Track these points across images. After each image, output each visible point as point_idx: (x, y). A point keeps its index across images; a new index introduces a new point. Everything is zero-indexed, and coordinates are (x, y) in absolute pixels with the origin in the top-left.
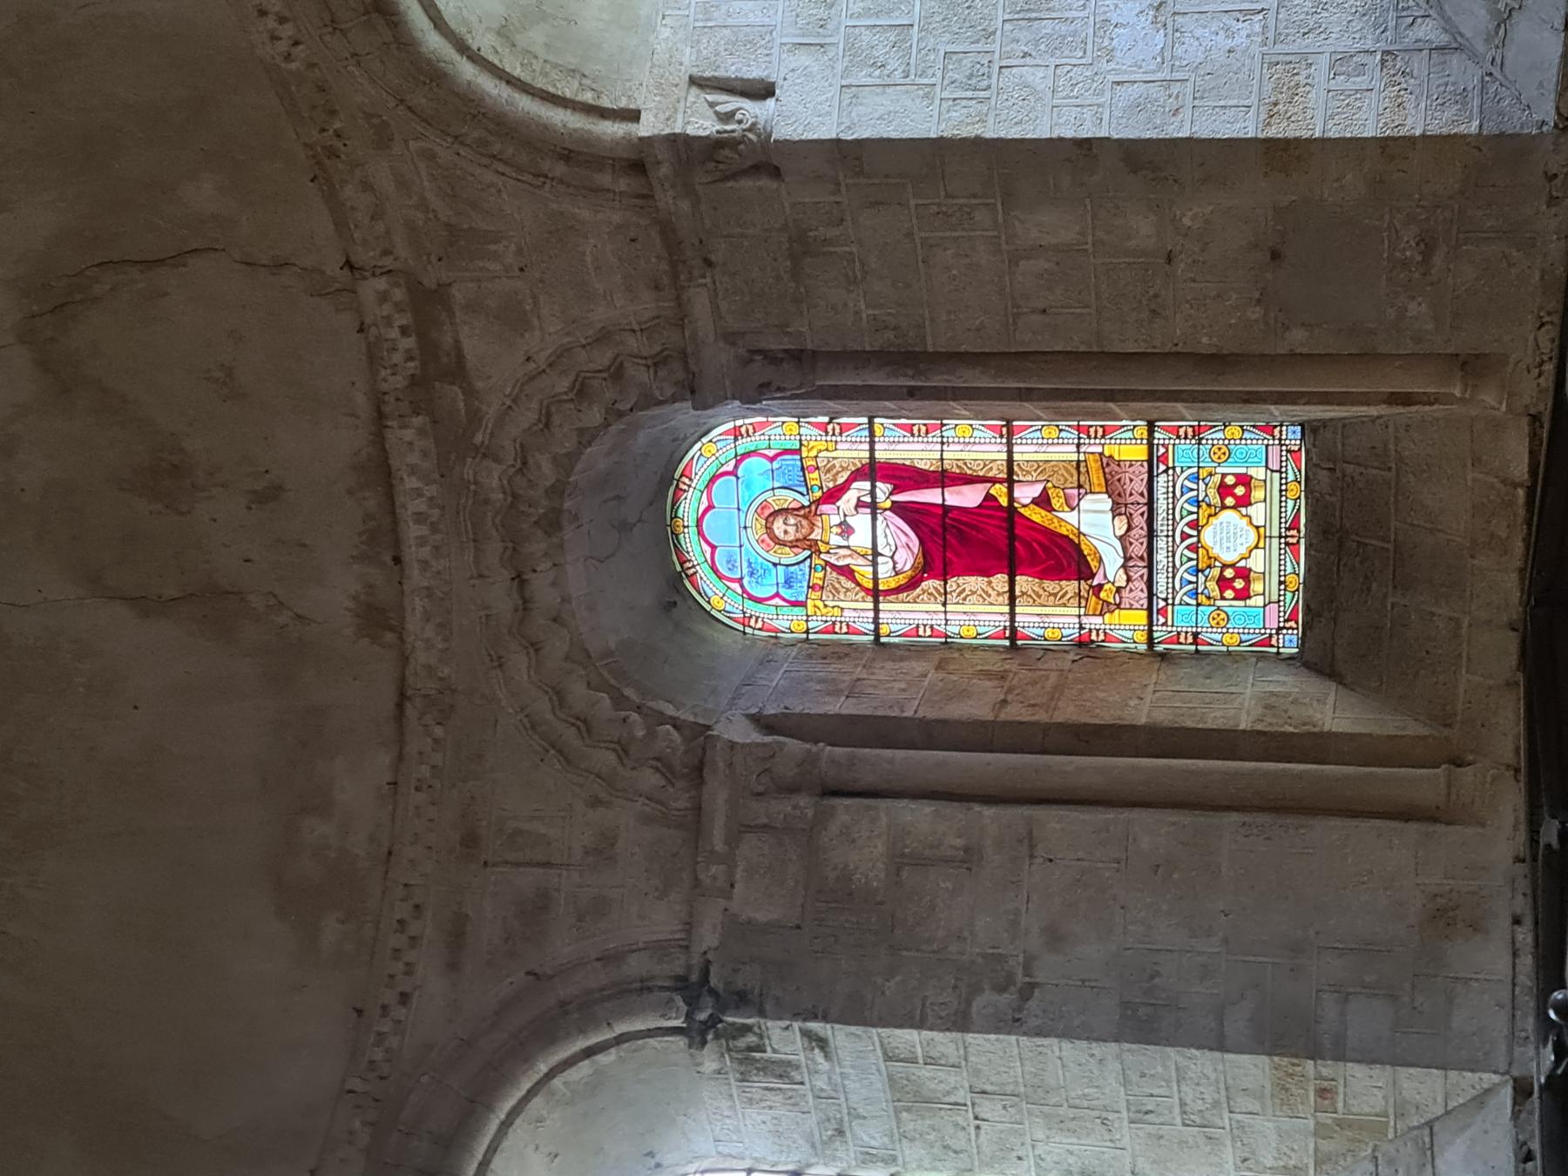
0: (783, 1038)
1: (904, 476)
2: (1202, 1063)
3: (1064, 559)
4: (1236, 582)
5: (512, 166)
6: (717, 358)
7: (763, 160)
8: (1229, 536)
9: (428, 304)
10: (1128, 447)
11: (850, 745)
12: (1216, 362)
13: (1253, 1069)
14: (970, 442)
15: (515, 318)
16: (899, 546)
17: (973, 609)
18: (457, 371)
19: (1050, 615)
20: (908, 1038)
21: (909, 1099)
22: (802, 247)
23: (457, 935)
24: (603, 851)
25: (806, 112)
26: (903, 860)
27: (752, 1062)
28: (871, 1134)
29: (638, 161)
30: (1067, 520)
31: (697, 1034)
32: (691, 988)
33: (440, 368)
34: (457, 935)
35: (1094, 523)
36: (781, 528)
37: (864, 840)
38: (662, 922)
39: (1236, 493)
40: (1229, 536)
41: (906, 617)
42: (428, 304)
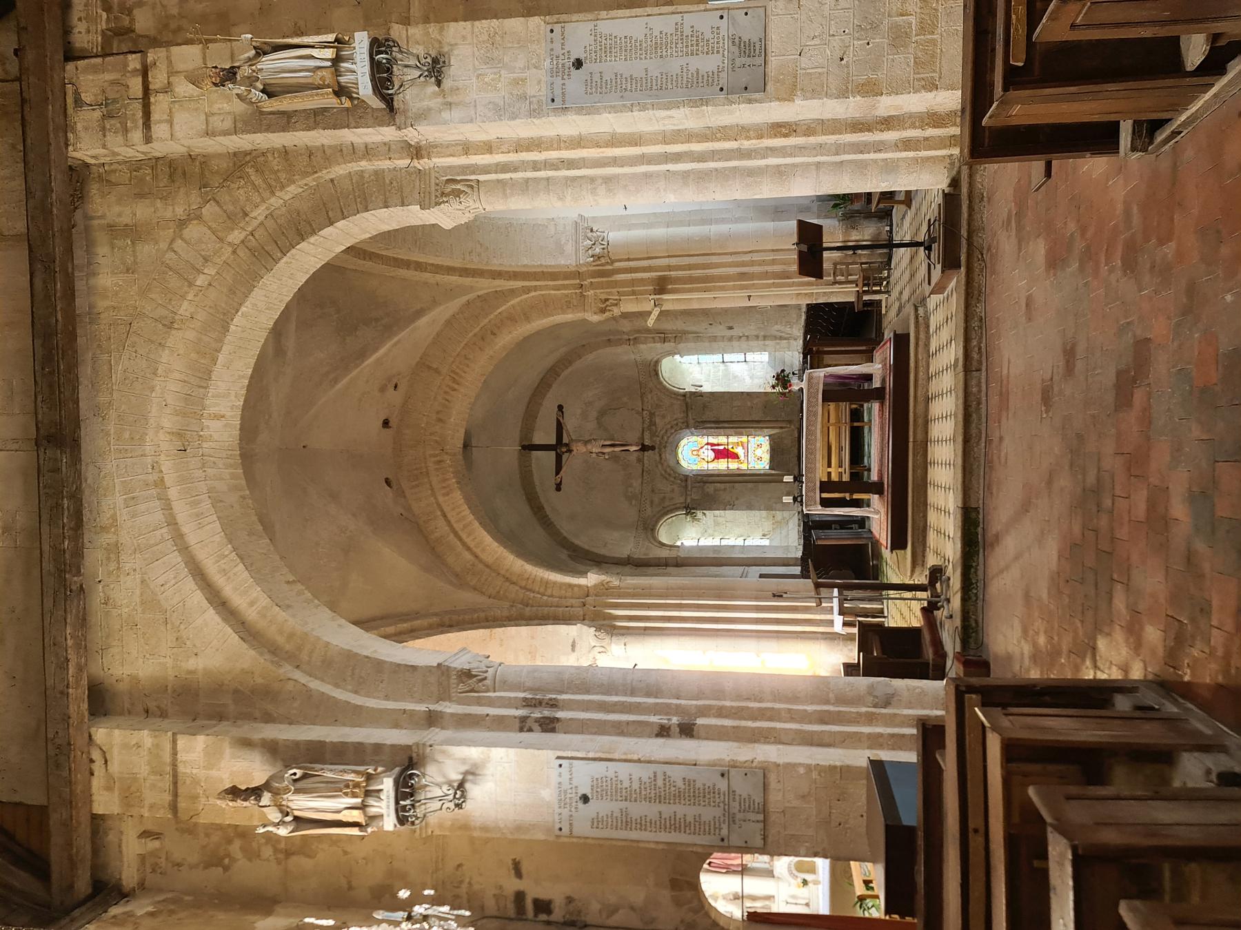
0: (699, 514)
1: (713, 445)
2: (757, 513)
3: (735, 456)
4: (760, 459)
5: (970, 201)
6: (691, 422)
7: (701, 395)
8: (759, 452)
9: (652, 415)
10: (744, 439)
11: (704, 480)
12: (758, 422)
13: (764, 513)
14: (722, 439)
15: (664, 417)
16: (712, 455)
17: (722, 465)
18: (655, 424)
19: (733, 465)
20: (717, 512)
21: (717, 524)
22: (705, 407)
23: (652, 502)
24: (673, 491)
25: (707, 388)
26: (715, 490)
27: (694, 518)
28: (710, 531)
29: (684, 395)
30: (735, 451)
31: (687, 514)
32: (686, 508)
33: (652, 423)
34: (652, 502)
35: (740, 451)
36: (694, 453)
37: (710, 488)
38: (682, 500)
39: (760, 446)
40: (759, 452)
41: (712, 466)
42: (652, 415)
